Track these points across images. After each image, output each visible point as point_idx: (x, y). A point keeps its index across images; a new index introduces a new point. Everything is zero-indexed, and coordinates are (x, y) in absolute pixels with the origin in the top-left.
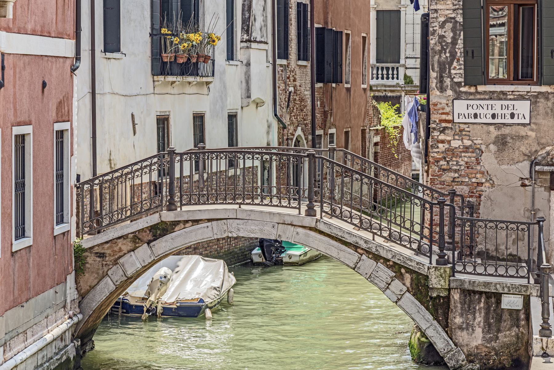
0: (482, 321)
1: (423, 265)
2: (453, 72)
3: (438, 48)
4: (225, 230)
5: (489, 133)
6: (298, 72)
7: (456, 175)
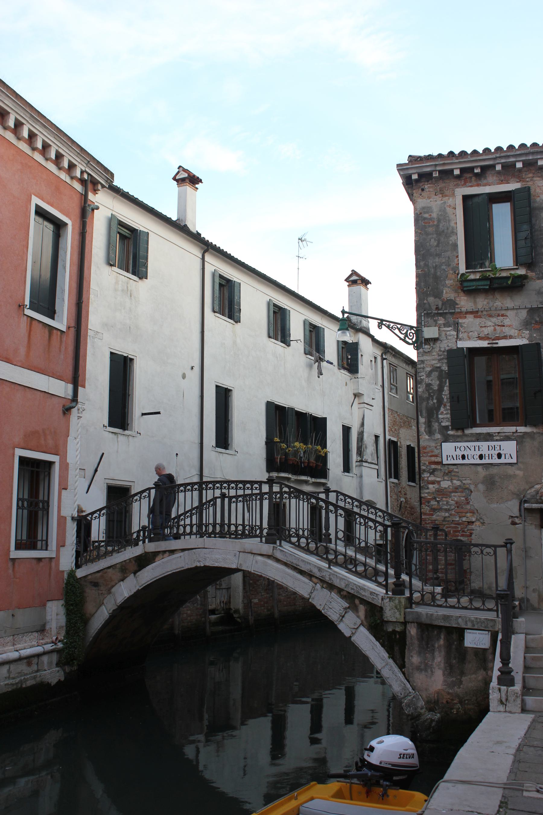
0: (443, 661)
1: (377, 594)
2: (440, 416)
3: (426, 395)
4: (195, 560)
5: (477, 473)
6: (408, 489)
7: (447, 514)
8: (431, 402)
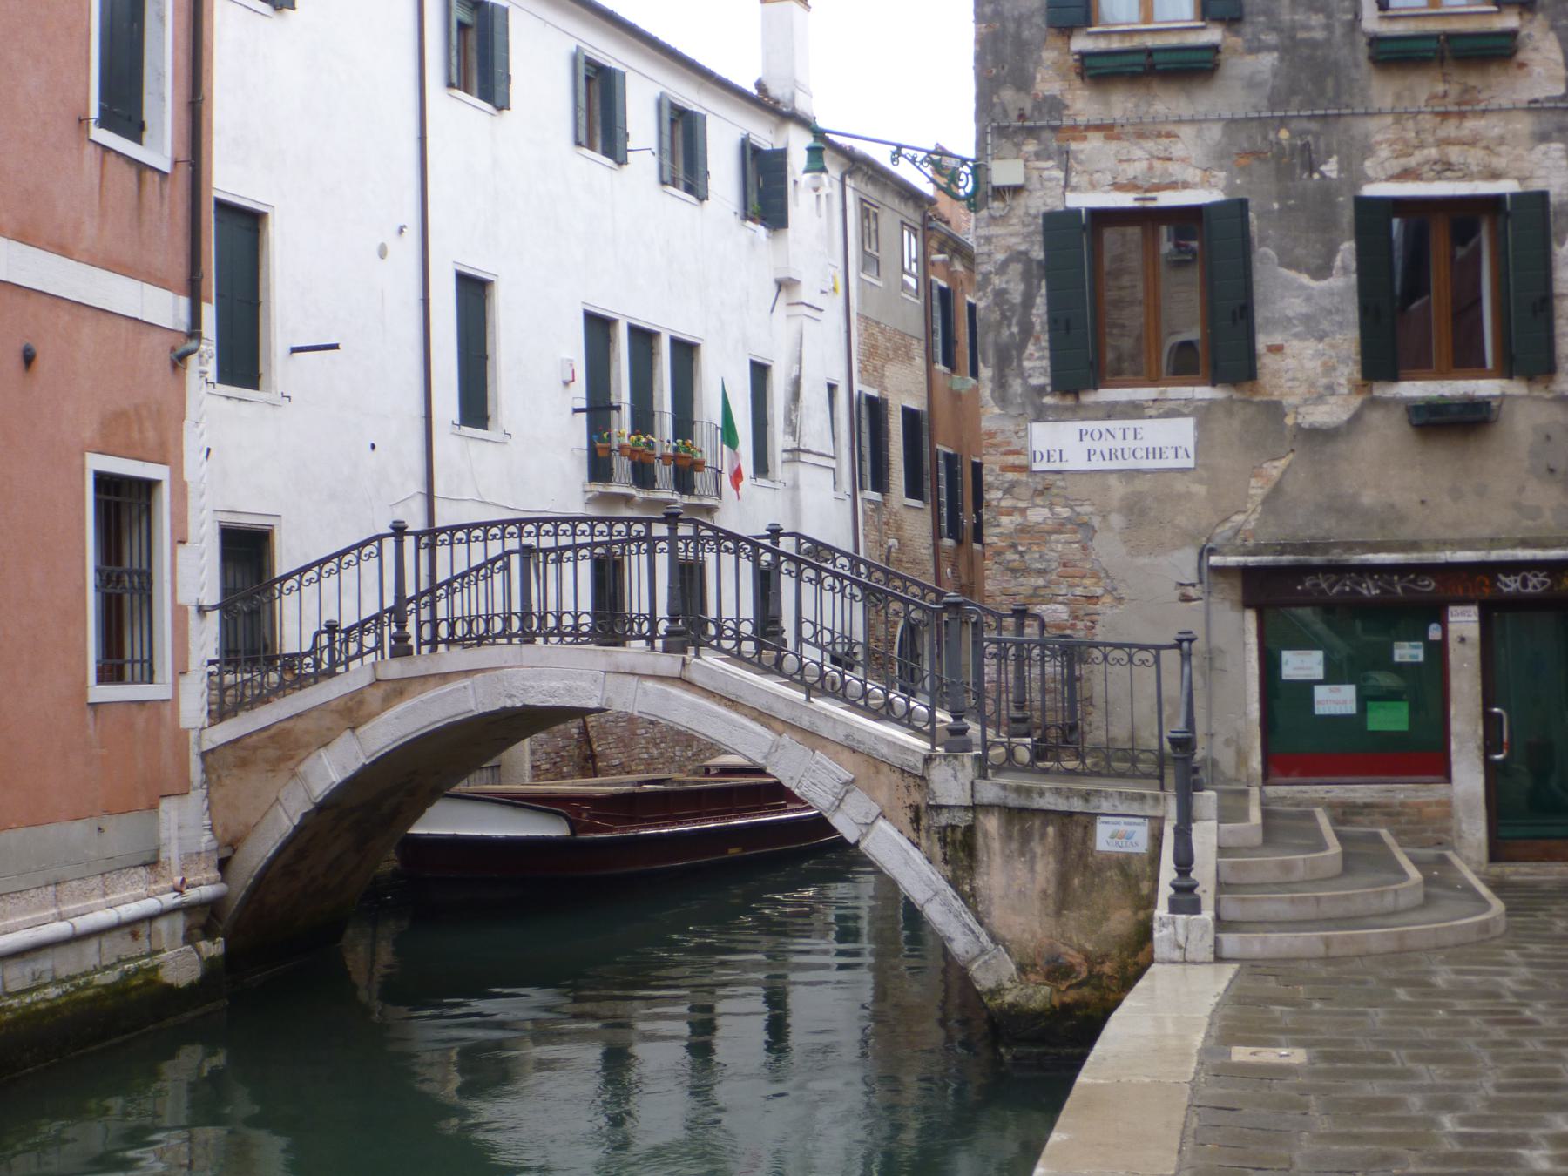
2: (1026, 364)
7: (1041, 582)
8: (1005, 333)
